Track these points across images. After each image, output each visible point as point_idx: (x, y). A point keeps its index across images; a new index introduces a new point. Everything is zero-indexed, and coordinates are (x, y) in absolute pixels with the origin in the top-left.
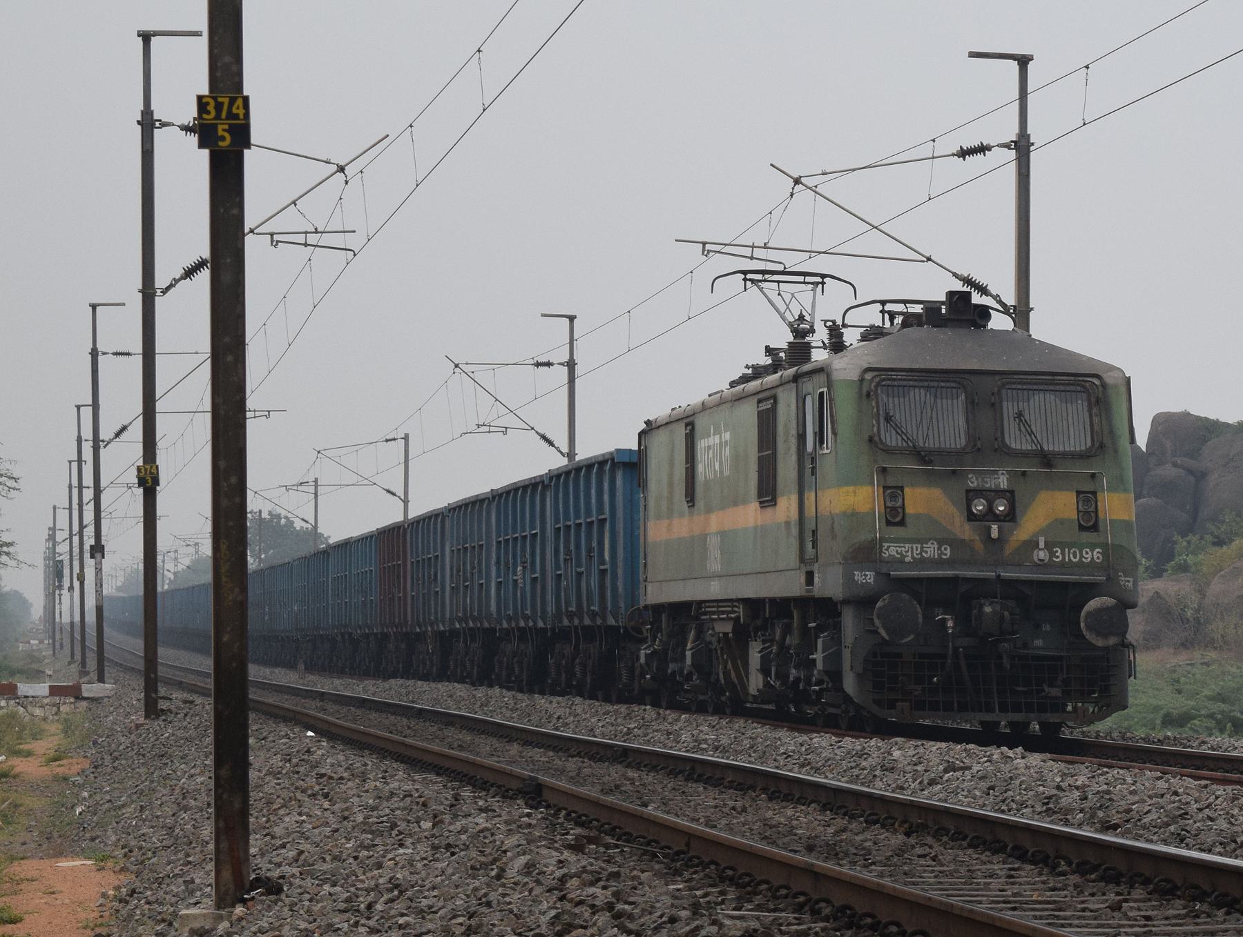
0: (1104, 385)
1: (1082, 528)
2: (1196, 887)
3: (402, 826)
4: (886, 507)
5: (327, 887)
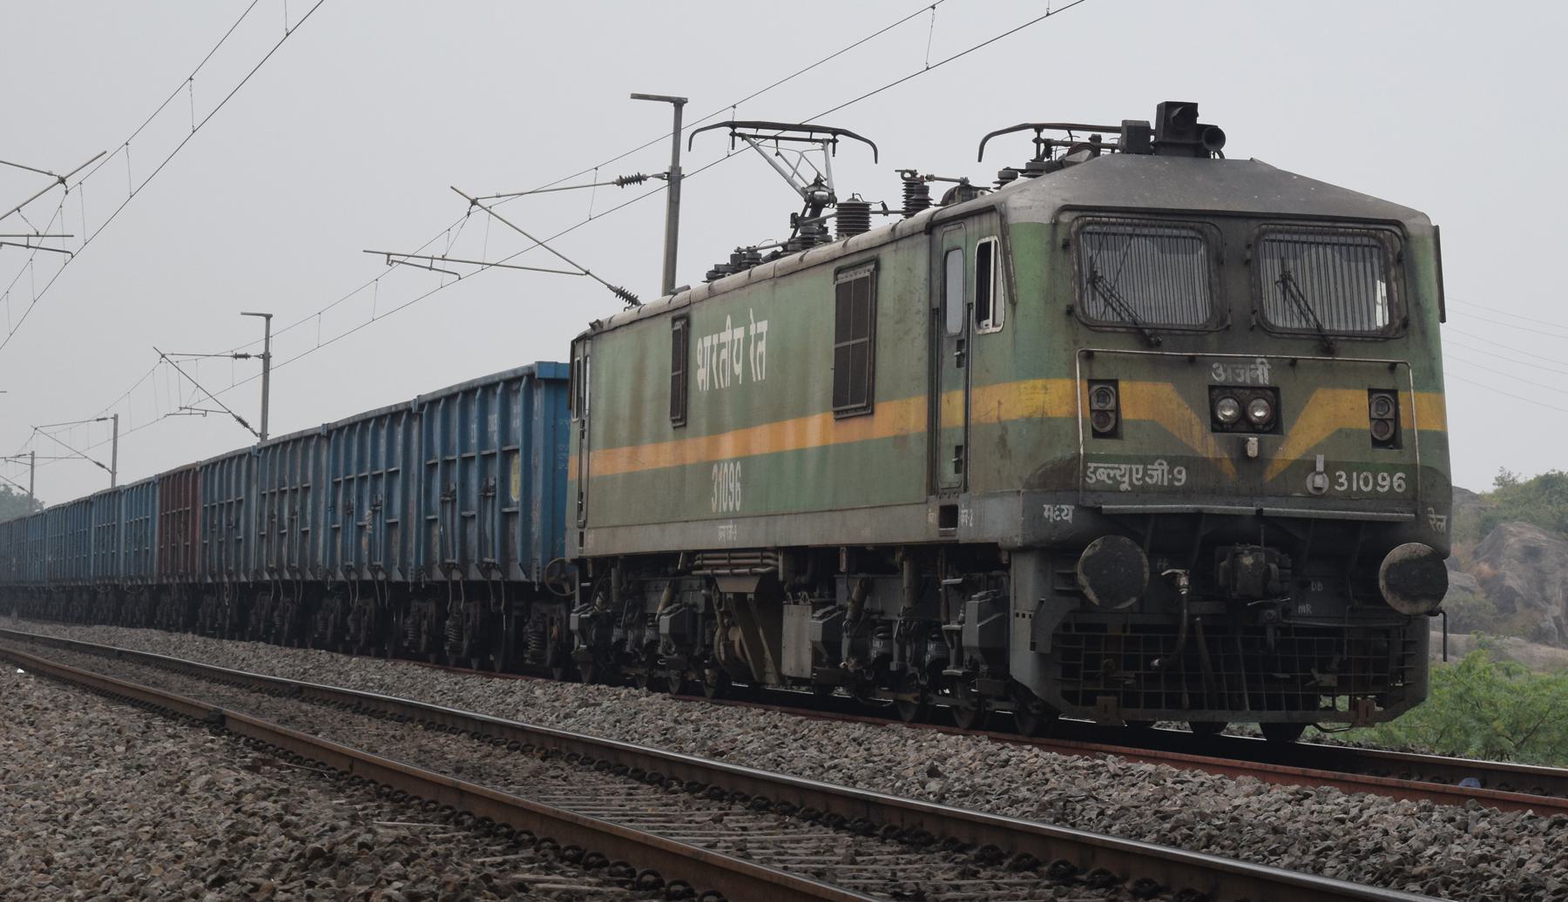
0: (1406, 237)
1: (1376, 443)
2: (787, 803)
3: (99, 749)
4: (1092, 411)
5: (29, 801)
